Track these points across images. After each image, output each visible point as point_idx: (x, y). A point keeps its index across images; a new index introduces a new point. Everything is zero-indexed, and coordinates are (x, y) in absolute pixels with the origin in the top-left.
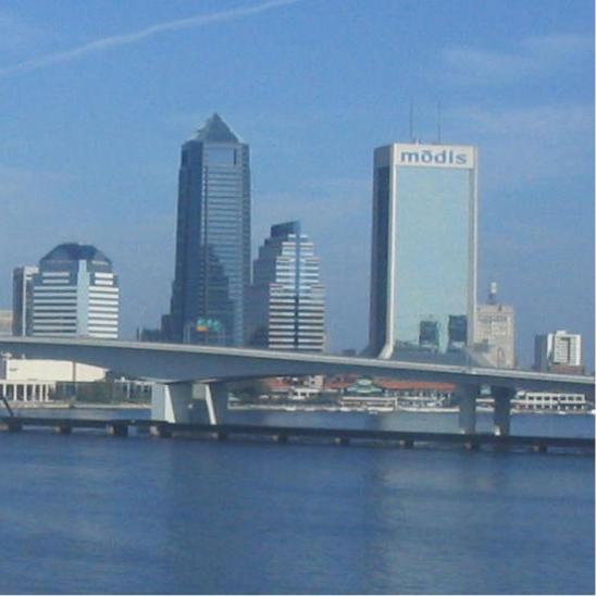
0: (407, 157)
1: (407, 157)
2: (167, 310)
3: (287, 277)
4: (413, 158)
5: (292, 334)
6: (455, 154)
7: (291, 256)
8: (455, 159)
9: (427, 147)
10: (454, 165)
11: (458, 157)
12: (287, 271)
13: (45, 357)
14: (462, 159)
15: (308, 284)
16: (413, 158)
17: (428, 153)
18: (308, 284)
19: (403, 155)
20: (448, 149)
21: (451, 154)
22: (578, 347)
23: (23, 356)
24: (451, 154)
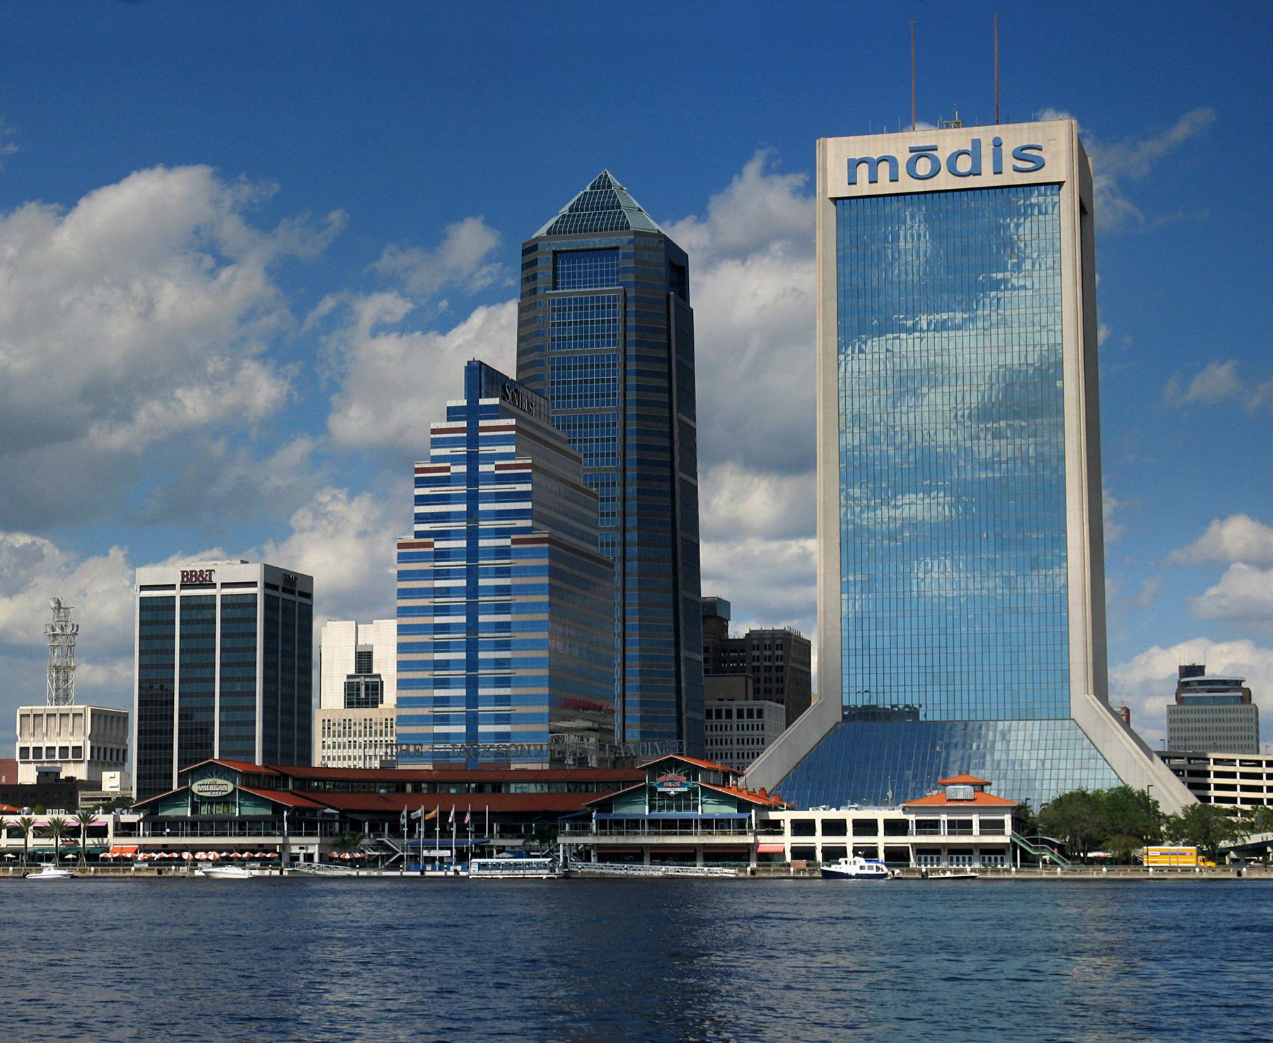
0: (863, 170)
1: (863, 170)
2: (159, 171)
3: (500, 497)
4: (884, 169)
5: (461, 526)
6: (1007, 150)
7: (455, 460)
8: (1008, 162)
9: (922, 135)
10: (1009, 178)
11: (1019, 154)
12: (500, 497)
13: (1098, 428)
14: (1029, 156)
15: (500, 533)
16: (884, 169)
17: (921, 152)
18: (500, 533)
19: (854, 165)
20: (986, 134)
21: (998, 144)
22: (442, 709)
23: (243, 177)
24: (998, 144)
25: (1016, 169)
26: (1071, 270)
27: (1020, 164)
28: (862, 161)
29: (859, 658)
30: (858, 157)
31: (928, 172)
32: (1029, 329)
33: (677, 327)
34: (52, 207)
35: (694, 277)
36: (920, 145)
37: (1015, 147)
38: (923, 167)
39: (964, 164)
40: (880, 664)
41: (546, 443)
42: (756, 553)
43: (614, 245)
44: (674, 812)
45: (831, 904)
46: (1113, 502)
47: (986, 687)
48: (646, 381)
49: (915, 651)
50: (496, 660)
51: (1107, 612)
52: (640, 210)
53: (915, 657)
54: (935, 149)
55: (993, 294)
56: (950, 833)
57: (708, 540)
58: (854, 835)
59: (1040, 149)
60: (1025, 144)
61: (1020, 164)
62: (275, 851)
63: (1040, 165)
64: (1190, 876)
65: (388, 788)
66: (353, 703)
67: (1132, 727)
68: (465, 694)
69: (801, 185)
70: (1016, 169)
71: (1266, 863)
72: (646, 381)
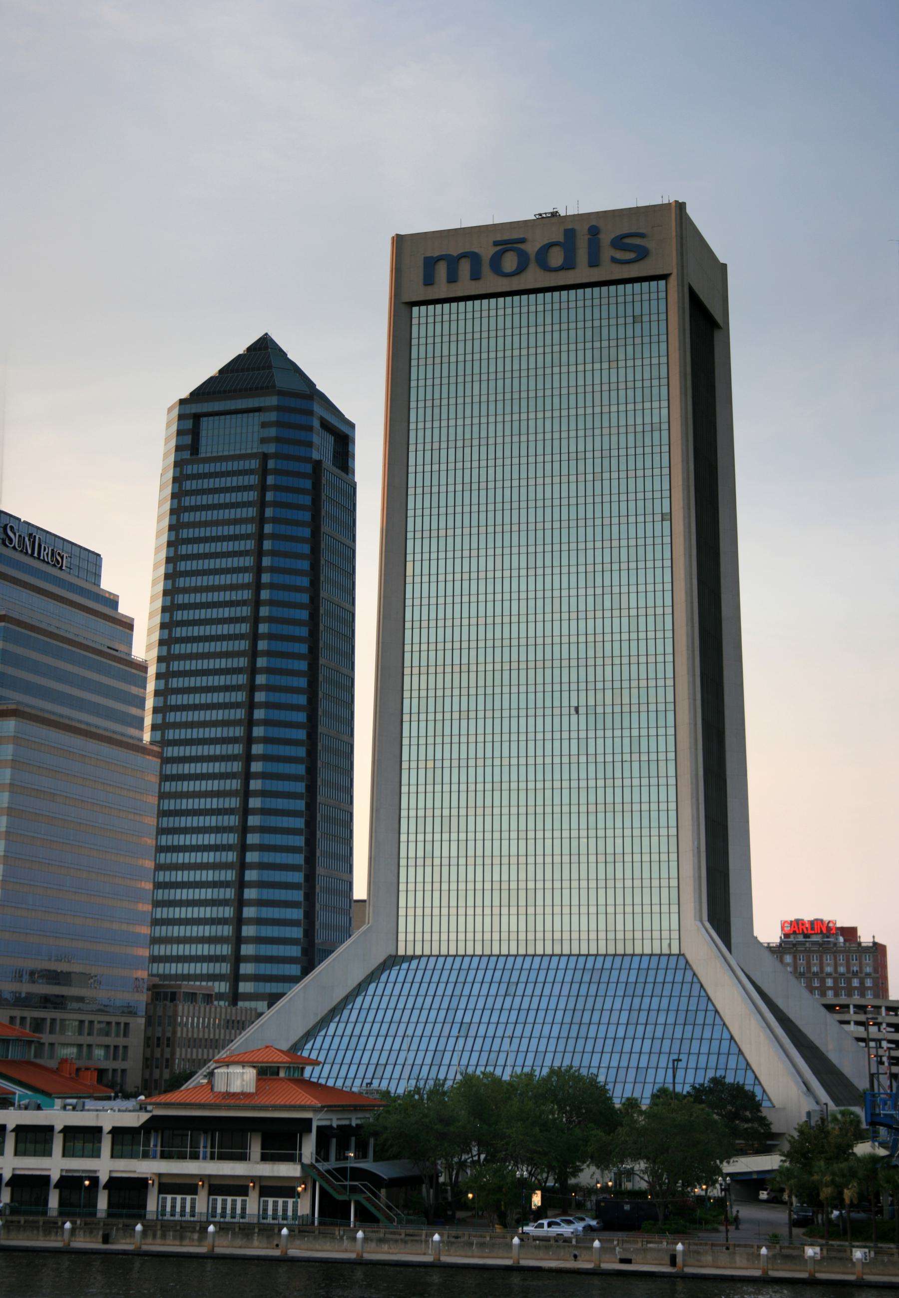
0: (442, 270)
1: (442, 270)
4: (465, 267)
8: (607, 252)
16: (465, 267)
25: (614, 260)
26: (122, 1169)
27: (619, 255)
28: (440, 258)
29: (540, 672)
30: (436, 254)
31: (514, 268)
32: (506, 1046)
33: (246, 1039)
34: (856, 1195)
35: (397, 1162)
36: (506, 238)
37: (613, 236)
38: (510, 262)
39: (556, 258)
40: (516, 360)
41: (110, 741)
42: (328, 1244)
43: (521, 236)
44: (740, 1260)
45: (569, 1222)
46: (580, 1229)
47: (467, 443)
48: (302, 435)
49: (608, 661)
50: (58, 984)
51: (729, 800)
52: (628, 1261)
53: (540, 364)
54: (522, 241)
55: (216, 1003)
56: (265, 1158)
57: (301, 830)
58: (64, 1155)
59: (642, 236)
60: (626, 231)
61: (619, 255)
62: (524, 1237)
63: (643, 254)
64: (257, 1248)
65: (530, 1162)
66: (619, 243)
67: (332, 439)
68: (190, 442)
69: (607, 1087)
70: (614, 260)
71: (896, 1015)
72: (302, 435)
